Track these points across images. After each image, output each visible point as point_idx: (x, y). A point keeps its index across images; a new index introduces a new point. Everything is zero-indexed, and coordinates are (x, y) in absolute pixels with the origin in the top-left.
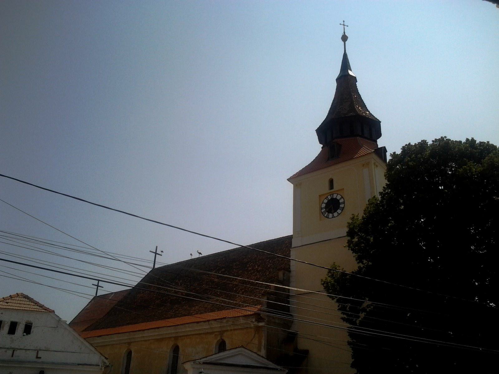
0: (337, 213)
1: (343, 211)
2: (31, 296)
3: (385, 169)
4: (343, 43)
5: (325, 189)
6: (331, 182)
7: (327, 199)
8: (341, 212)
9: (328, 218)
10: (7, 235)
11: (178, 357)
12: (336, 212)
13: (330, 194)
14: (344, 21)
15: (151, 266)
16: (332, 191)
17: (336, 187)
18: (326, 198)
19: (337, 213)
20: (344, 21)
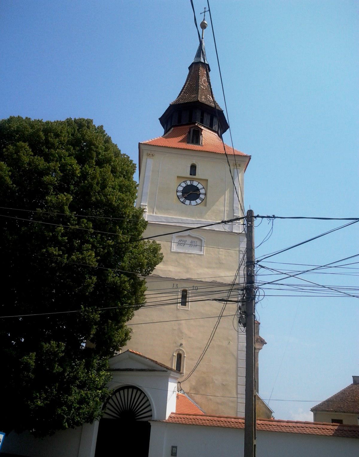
0: (196, 202)
1: (177, 197)
2: (211, 84)
3: (233, 160)
4: (202, 30)
5: (187, 173)
6: (193, 168)
7: (186, 183)
8: (180, 201)
9: (184, 204)
10: (204, 295)
11: (136, 369)
12: (195, 201)
13: (190, 180)
14: (201, 14)
15: (166, 306)
16: (194, 177)
17: (199, 173)
18: (184, 182)
19: (196, 202)
20: (201, 14)
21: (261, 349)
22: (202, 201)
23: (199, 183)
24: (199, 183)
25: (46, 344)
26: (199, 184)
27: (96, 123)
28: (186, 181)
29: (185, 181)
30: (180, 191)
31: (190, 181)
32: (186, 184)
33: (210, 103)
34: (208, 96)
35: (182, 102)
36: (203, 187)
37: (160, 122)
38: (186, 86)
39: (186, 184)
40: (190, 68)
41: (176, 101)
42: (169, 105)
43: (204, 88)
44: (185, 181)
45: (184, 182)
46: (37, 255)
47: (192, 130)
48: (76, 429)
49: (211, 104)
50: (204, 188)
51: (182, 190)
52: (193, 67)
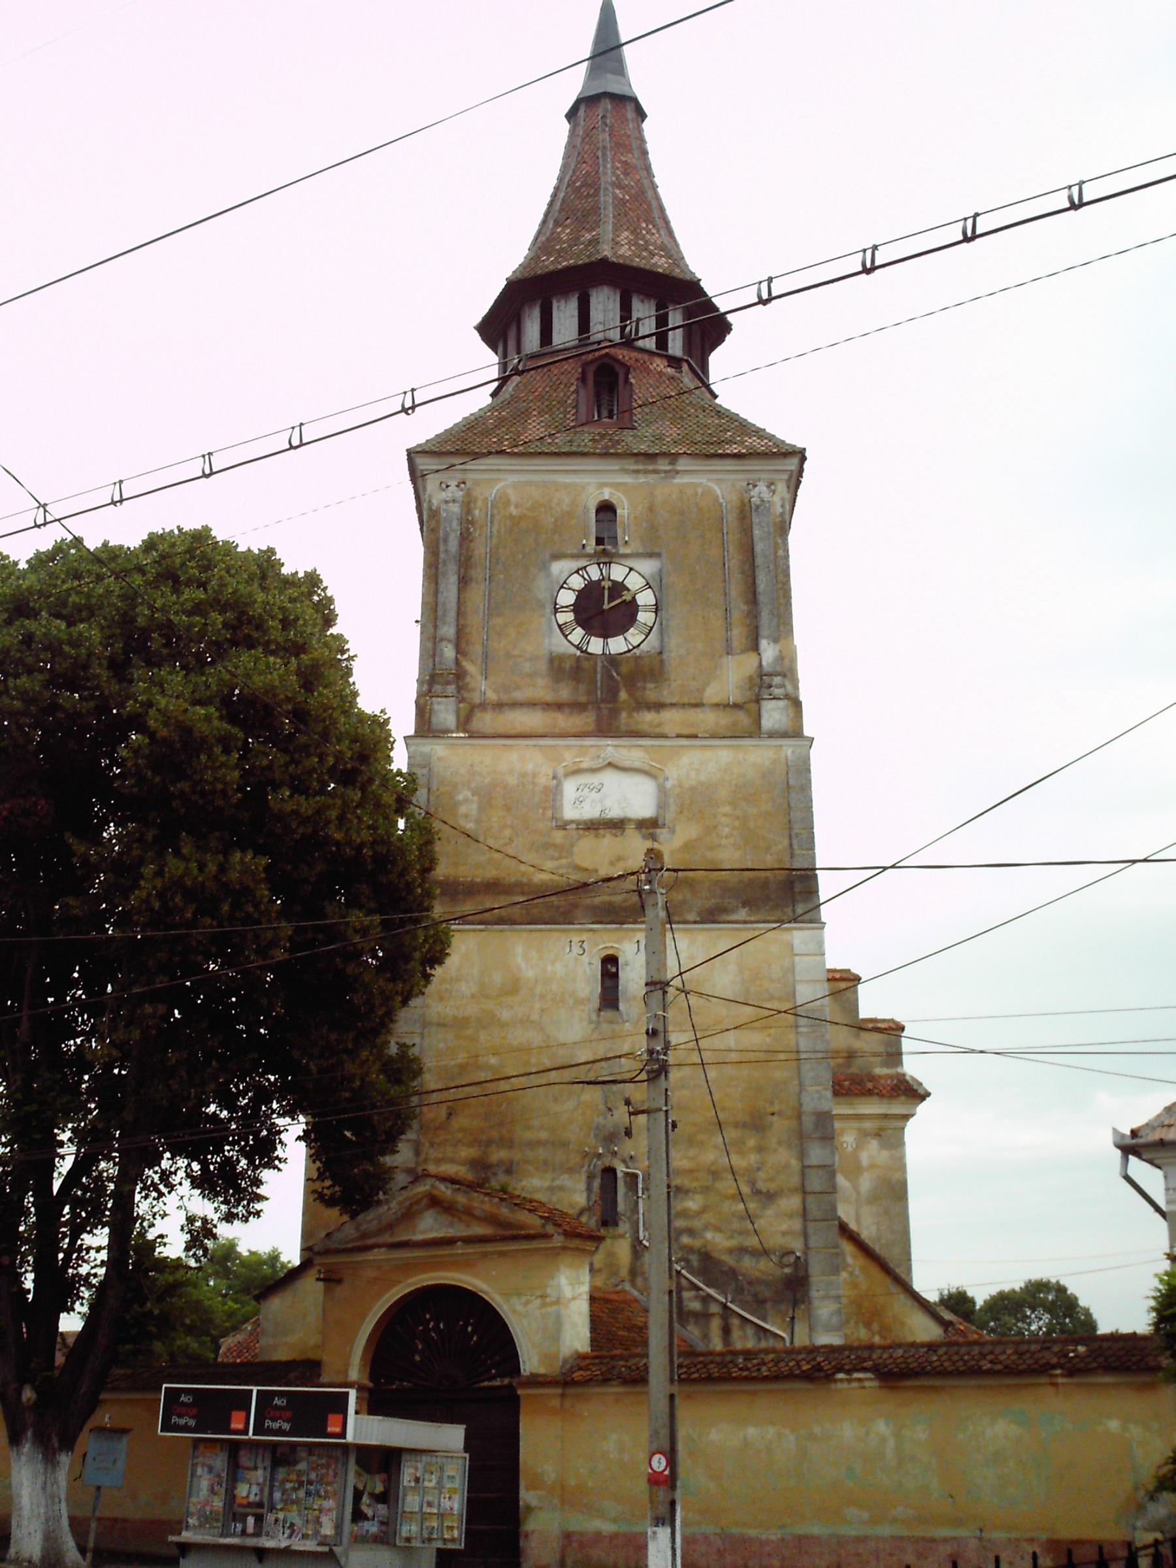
18: (577, 572)
21: (913, 1115)
22: (647, 637)
23: (631, 569)
24: (631, 569)
25: (172, 595)
26: (632, 572)
27: (293, 564)
28: (585, 568)
29: (581, 569)
30: (567, 607)
31: (599, 564)
32: (585, 579)
33: (653, 255)
34: (644, 225)
35: (550, 263)
36: (648, 584)
37: (479, 338)
38: (562, 195)
39: (585, 579)
40: (571, 115)
41: (534, 258)
42: (505, 283)
43: (627, 197)
44: (581, 569)
45: (577, 572)
46: (247, 1082)
47: (592, 369)
48: (439, 839)
49: (656, 258)
50: (650, 587)
51: (572, 602)
52: (581, 113)
